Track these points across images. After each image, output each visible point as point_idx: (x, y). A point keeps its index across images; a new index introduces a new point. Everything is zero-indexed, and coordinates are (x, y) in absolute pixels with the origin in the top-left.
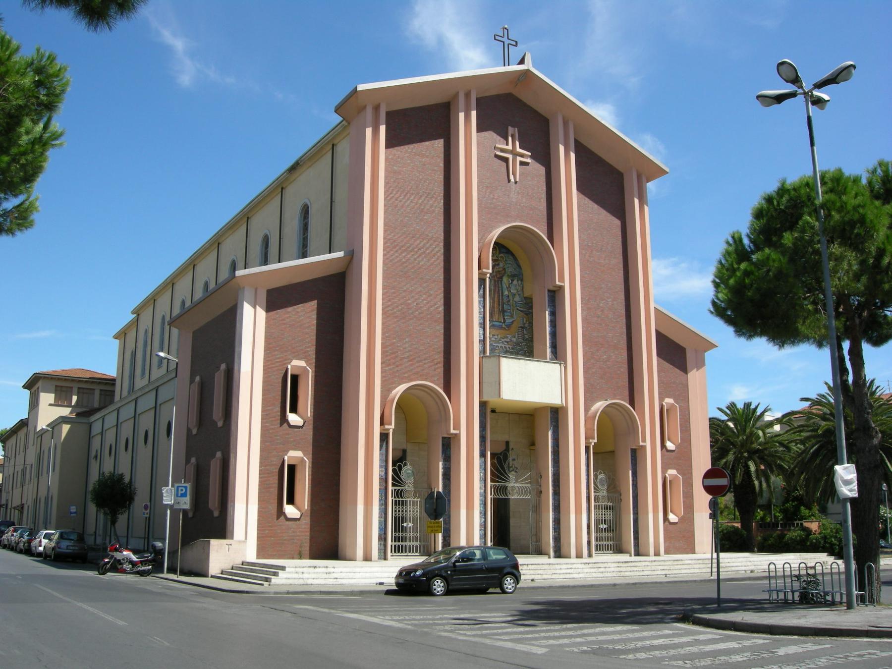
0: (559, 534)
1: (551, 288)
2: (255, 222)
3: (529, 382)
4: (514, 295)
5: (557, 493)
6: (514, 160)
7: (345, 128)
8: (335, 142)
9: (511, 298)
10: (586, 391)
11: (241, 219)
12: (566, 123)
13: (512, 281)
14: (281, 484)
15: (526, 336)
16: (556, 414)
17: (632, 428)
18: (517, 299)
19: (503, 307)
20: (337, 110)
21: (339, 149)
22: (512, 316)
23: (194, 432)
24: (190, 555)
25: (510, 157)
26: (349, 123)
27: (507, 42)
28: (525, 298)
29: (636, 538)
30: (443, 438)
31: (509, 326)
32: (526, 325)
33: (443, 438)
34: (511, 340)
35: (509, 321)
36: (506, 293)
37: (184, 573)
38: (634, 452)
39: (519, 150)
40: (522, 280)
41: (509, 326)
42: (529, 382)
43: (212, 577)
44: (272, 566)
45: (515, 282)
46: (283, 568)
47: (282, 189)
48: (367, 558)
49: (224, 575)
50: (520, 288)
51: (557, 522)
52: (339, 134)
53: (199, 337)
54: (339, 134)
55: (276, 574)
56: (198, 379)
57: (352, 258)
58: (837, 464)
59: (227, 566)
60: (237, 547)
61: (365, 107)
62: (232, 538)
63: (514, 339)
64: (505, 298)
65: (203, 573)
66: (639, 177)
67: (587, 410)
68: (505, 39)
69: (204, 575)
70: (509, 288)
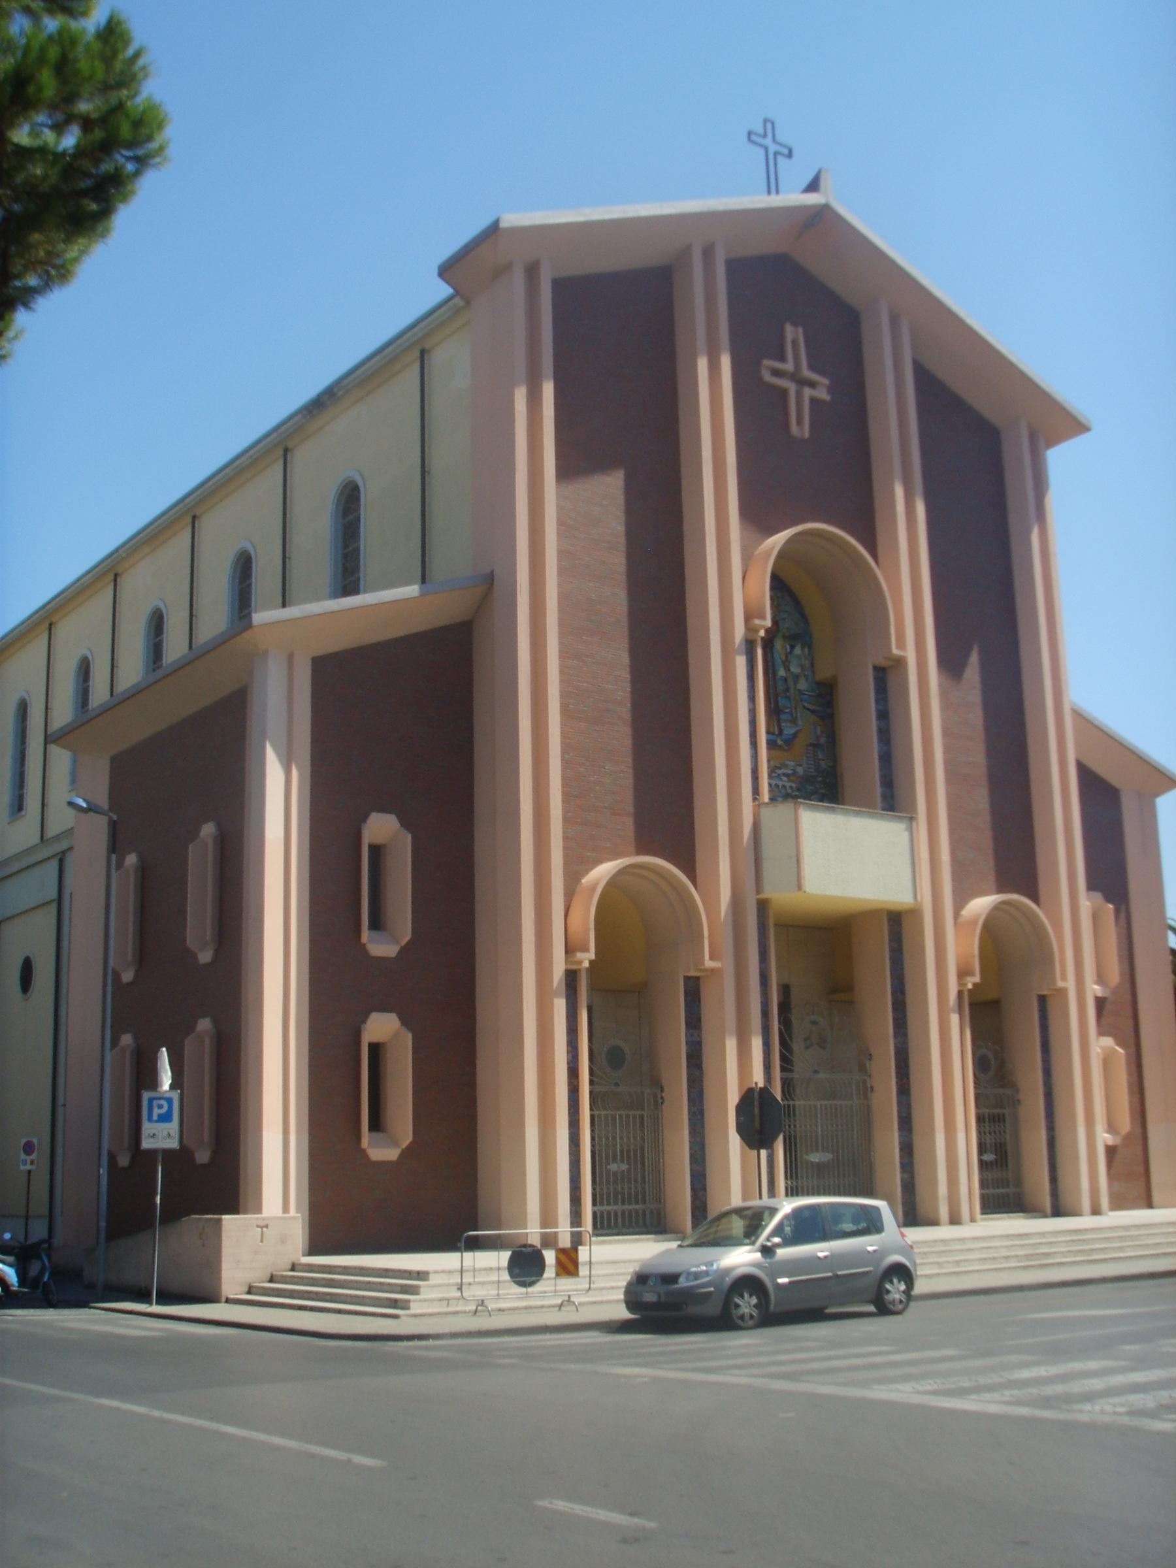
0: (912, 1177)
1: (881, 662)
2: (66, 630)
3: (851, 859)
4: (796, 677)
5: (904, 1090)
6: (799, 396)
7: (458, 311)
8: (427, 346)
9: (791, 683)
10: (956, 876)
11: (38, 624)
12: (894, 321)
13: (792, 647)
14: (341, 1087)
15: (823, 764)
16: (897, 924)
17: (1040, 953)
18: (803, 685)
19: (777, 703)
20: (445, 271)
21: (439, 357)
22: (794, 721)
23: (128, 976)
24: (161, 1251)
25: (792, 387)
26: (468, 303)
27: (773, 148)
28: (820, 684)
29: (1054, 1180)
30: (687, 979)
31: (789, 742)
32: (823, 740)
33: (687, 979)
34: (795, 772)
35: (789, 731)
36: (782, 672)
37: (166, 1297)
38: (1042, 999)
39: (807, 373)
40: (810, 647)
41: (789, 742)
42: (851, 859)
43: (228, 1301)
44: (407, 1274)
45: (798, 650)
46: (422, 1275)
47: (194, 518)
48: (973, 1220)
49: (254, 1295)
50: (807, 663)
51: (907, 1149)
52: (442, 325)
53: (128, 770)
54: (442, 325)
55: (414, 1290)
56: (131, 860)
57: (490, 588)
58: (193, 1159)
59: (256, 1274)
60: (267, 1231)
61: (508, 267)
62: (259, 1210)
63: (800, 770)
64: (780, 683)
65: (205, 1292)
66: (1033, 436)
67: (957, 915)
68: (768, 141)
69: (210, 1297)
70: (786, 664)
